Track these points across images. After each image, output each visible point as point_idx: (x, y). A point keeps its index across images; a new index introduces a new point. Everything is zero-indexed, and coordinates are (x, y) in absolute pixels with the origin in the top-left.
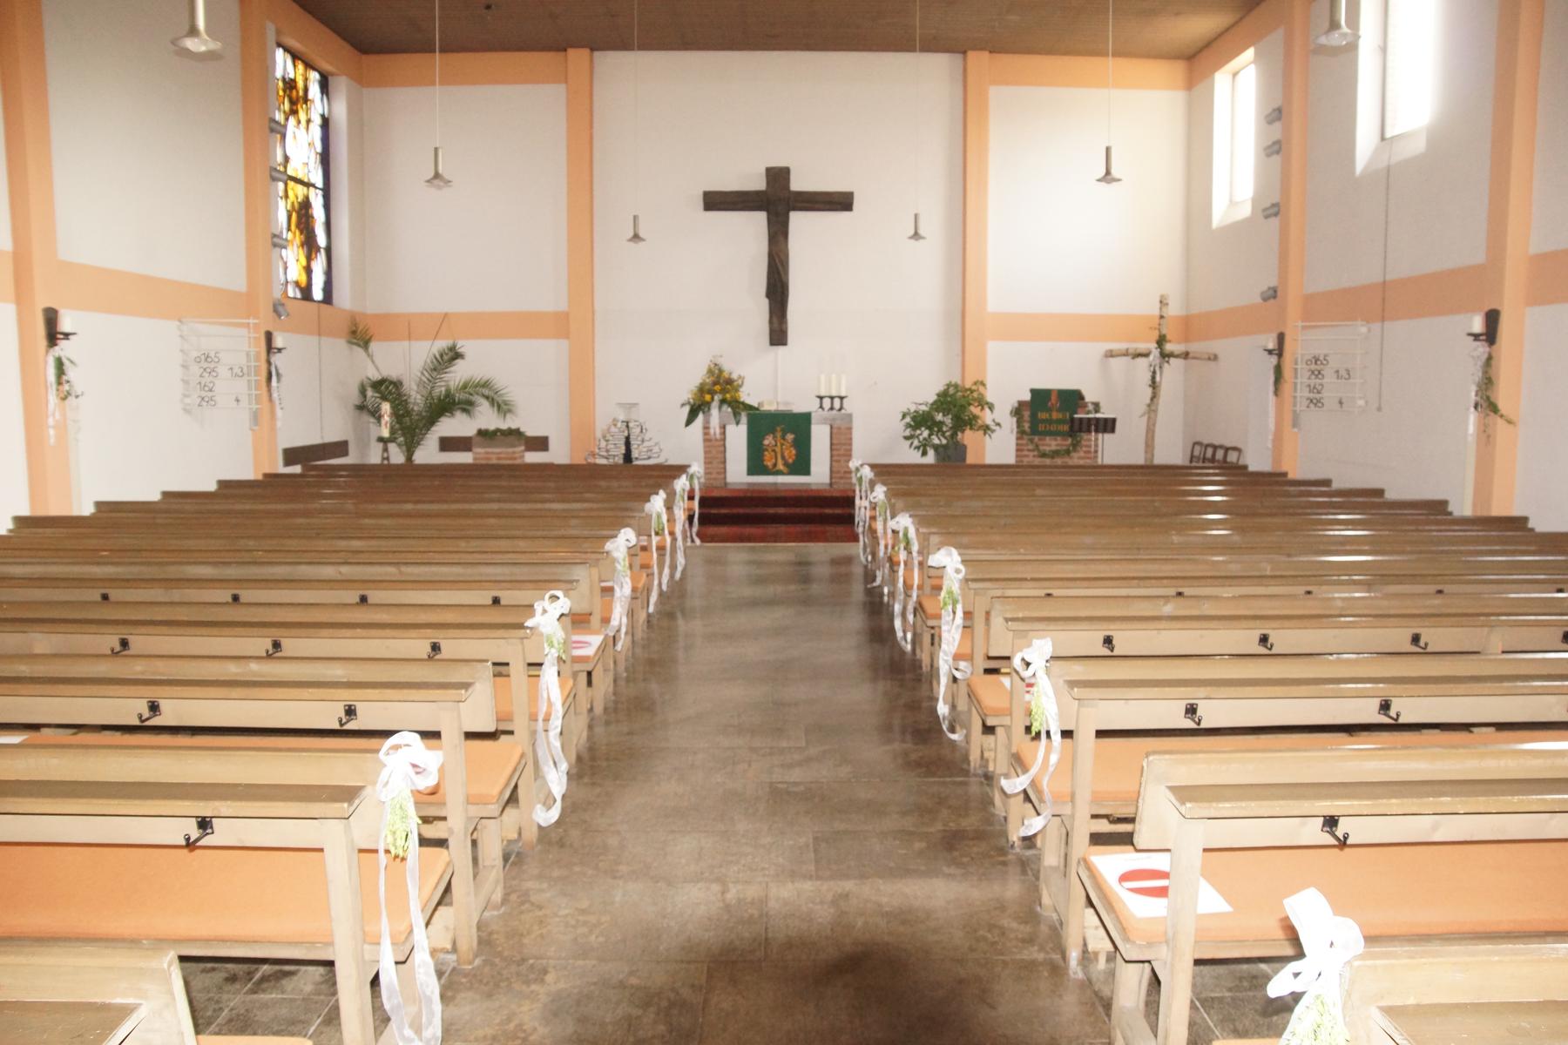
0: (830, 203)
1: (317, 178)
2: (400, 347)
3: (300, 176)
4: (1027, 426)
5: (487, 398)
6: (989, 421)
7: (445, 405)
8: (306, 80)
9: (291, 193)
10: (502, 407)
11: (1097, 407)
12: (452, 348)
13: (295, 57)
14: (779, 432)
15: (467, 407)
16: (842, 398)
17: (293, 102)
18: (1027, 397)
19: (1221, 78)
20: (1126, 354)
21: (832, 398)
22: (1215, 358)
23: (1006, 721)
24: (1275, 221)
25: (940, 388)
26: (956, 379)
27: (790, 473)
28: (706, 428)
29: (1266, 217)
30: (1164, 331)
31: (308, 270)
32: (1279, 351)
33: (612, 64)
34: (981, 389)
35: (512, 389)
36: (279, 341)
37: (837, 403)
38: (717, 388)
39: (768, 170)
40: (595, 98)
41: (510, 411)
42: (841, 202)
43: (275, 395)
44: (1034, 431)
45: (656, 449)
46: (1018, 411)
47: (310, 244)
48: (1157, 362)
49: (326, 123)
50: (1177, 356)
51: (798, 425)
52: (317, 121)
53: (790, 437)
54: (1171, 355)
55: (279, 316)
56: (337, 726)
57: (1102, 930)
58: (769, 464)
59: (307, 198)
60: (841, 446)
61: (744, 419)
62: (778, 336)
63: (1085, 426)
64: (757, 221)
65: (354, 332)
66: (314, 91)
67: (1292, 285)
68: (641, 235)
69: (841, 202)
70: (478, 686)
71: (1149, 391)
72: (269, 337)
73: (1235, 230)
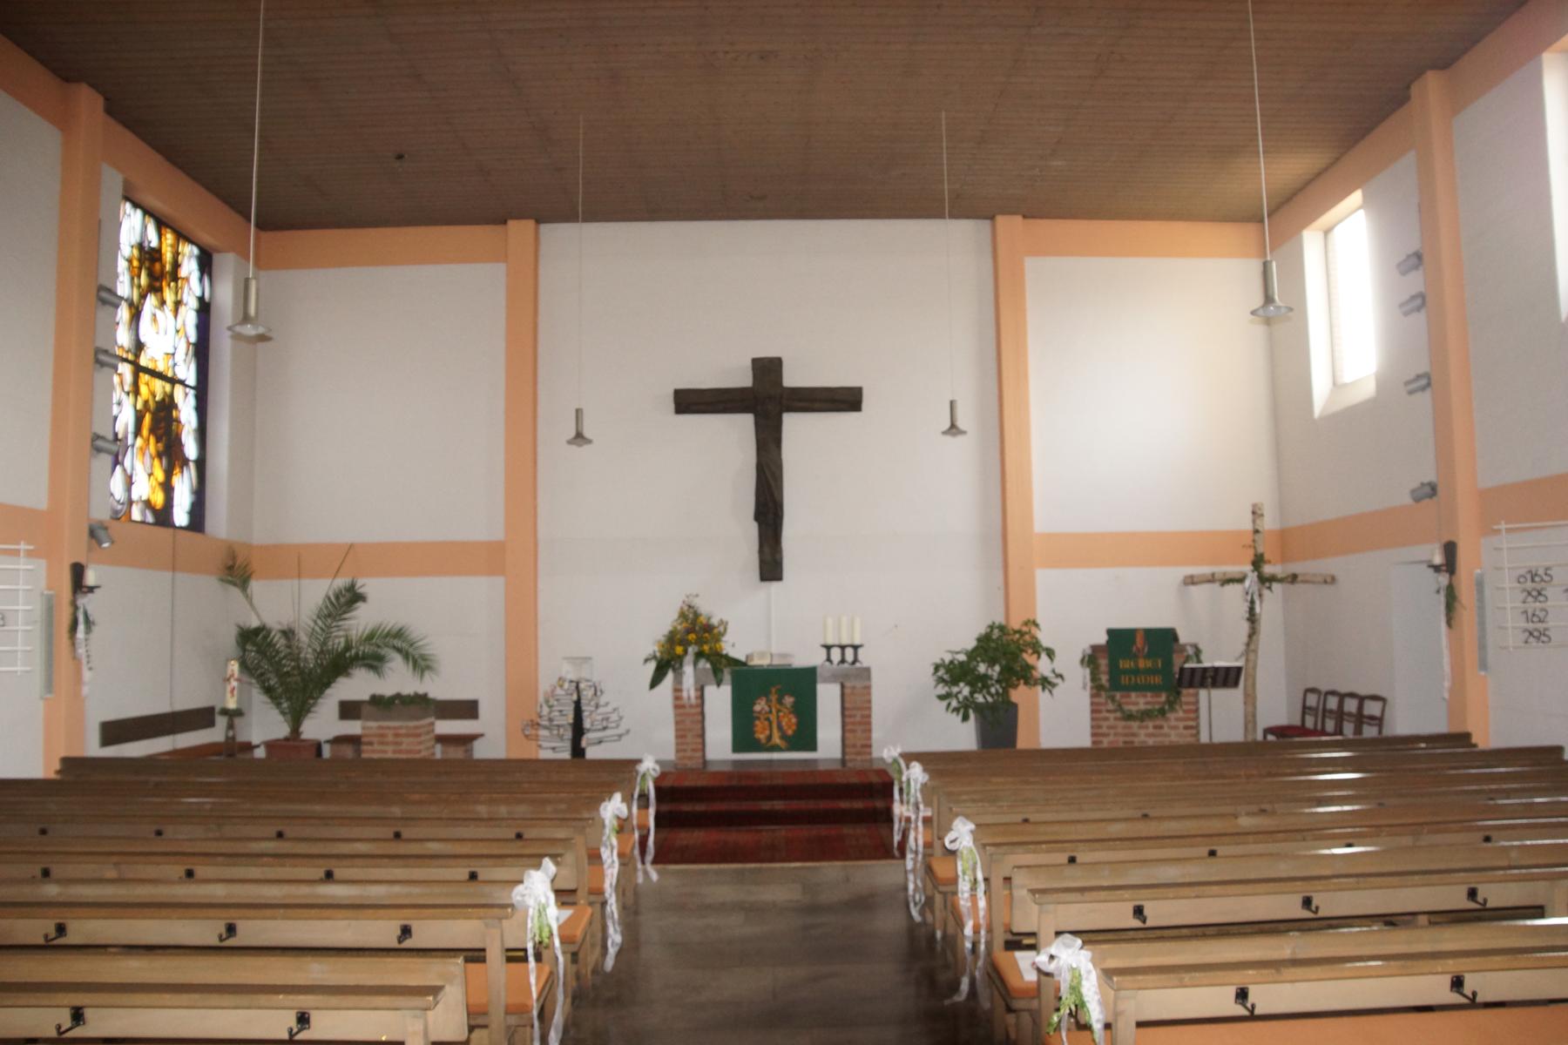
0: (833, 401)
1: (188, 373)
2: (288, 586)
3: (161, 367)
4: (1104, 679)
5: (399, 650)
6: (1048, 674)
7: (339, 664)
8: (176, 254)
9: (144, 390)
10: (420, 663)
11: (1198, 652)
12: (351, 588)
13: (161, 224)
14: (776, 693)
15: (374, 662)
16: (856, 648)
17: (151, 275)
18: (1102, 639)
19: (1311, 239)
20: (1211, 579)
21: (843, 648)
22: (1333, 580)
23: (1035, 1004)
24: (1425, 398)
25: (982, 629)
26: (999, 619)
27: (789, 749)
28: (677, 690)
29: (1411, 393)
30: (1260, 550)
31: (167, 488)
32: (1450, 564)
33: (558, 235)
34: (1034, 630)
35: (435, 643)
36: (90, 578)
37: (849, 653)
38: (692, 637)
39: (755, 361)
40: (541, 271)
41: (429, 668)
42: (847, 400)
43: (81, 651)
44: (1115, 685)
45: (614, 717)
46: (1091, 659)
47: (171, 454)
48: (1255, 588)
49: (204, 309)
50: (1281, 581)
52: (191, 303)
53: (789, 700)
54: (1273, 579)
55: (100, 543)
56: (395, 944)
58: (762, 737)
59: (171, 396)
60: (856, 716)
61: (727, 677)
62: (771, 568)
63: (1197, 678)
64: (741, 427)
65: (230, 568)
66: (189, 267)
67: (1417, 495)
68: (587, 434)
69: (847, 400)
70: (448, 988)
71: (1245, 627)
72: (78, 571)
73: (1350, 419)
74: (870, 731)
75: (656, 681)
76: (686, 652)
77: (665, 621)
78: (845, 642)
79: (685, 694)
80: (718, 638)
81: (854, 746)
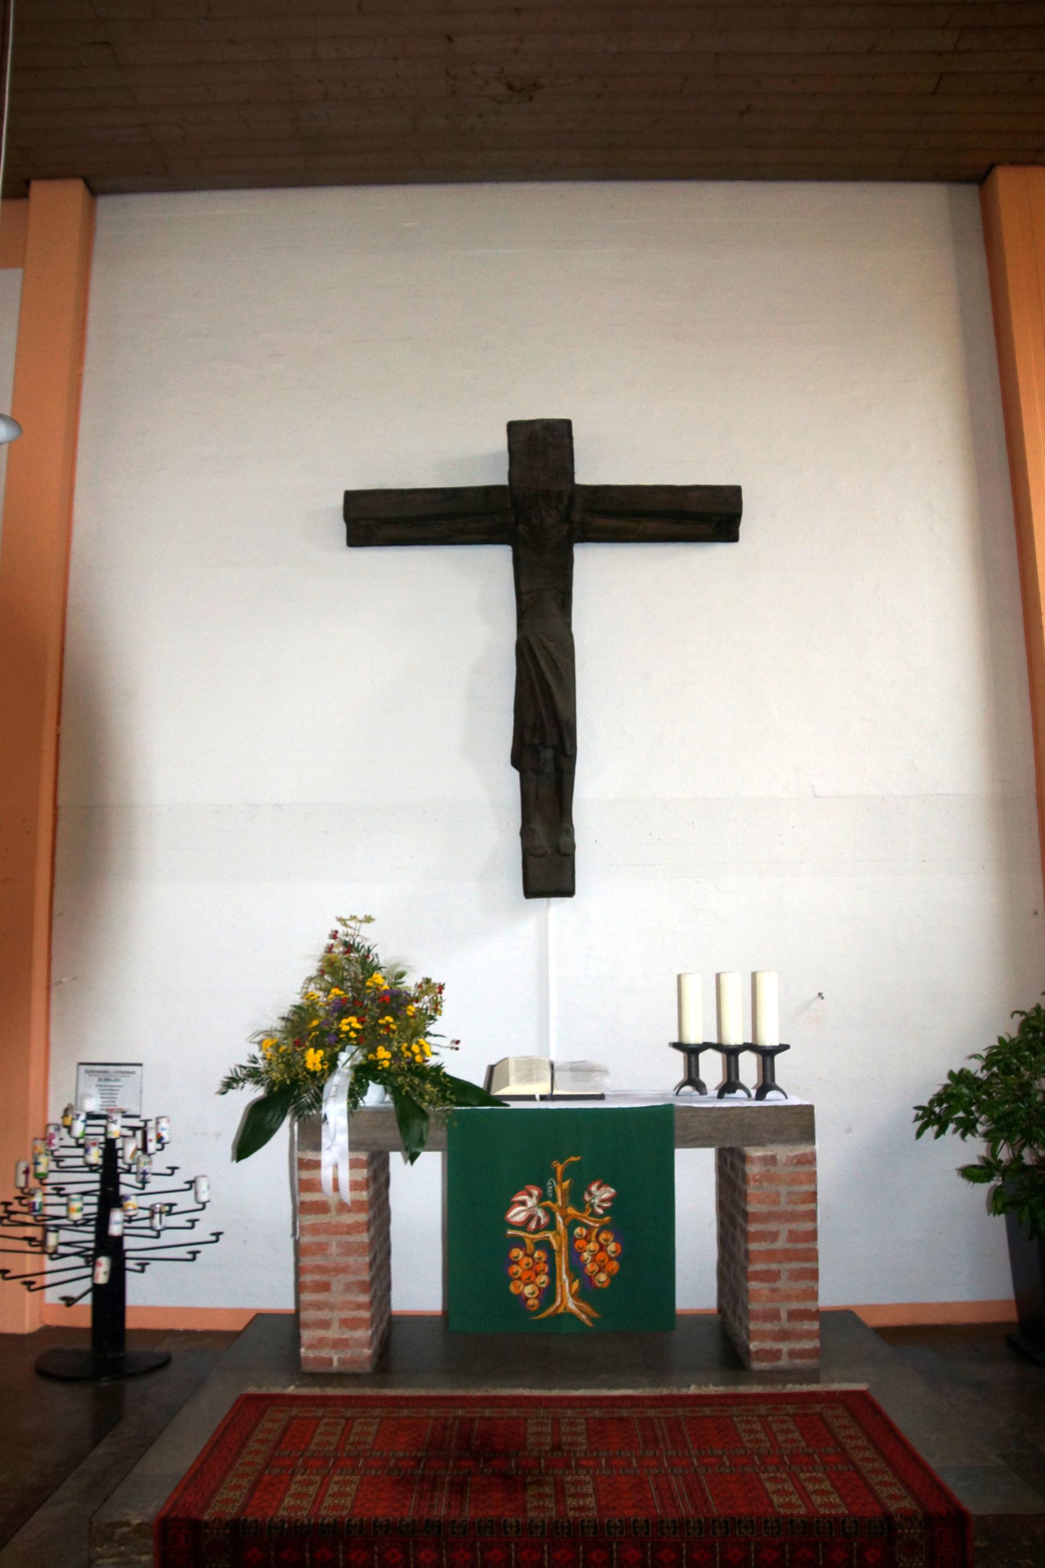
16: (767, 1055)
21: (731, 1053)
28: (304, 1165)
37: (749, 1066)
42: (705, 516)
51: (627, 1147)
53: (601, 1194)
57: (56, 912)
62: (548, 866)
69: (705, 516)
74: (814, 1275)
75: (250, 1139)
76: (332, 1063)
77: (285, 979)
78: (735, 1037)
79: (326, 1174)
80: (416, 1029)
81: (773, 1316)
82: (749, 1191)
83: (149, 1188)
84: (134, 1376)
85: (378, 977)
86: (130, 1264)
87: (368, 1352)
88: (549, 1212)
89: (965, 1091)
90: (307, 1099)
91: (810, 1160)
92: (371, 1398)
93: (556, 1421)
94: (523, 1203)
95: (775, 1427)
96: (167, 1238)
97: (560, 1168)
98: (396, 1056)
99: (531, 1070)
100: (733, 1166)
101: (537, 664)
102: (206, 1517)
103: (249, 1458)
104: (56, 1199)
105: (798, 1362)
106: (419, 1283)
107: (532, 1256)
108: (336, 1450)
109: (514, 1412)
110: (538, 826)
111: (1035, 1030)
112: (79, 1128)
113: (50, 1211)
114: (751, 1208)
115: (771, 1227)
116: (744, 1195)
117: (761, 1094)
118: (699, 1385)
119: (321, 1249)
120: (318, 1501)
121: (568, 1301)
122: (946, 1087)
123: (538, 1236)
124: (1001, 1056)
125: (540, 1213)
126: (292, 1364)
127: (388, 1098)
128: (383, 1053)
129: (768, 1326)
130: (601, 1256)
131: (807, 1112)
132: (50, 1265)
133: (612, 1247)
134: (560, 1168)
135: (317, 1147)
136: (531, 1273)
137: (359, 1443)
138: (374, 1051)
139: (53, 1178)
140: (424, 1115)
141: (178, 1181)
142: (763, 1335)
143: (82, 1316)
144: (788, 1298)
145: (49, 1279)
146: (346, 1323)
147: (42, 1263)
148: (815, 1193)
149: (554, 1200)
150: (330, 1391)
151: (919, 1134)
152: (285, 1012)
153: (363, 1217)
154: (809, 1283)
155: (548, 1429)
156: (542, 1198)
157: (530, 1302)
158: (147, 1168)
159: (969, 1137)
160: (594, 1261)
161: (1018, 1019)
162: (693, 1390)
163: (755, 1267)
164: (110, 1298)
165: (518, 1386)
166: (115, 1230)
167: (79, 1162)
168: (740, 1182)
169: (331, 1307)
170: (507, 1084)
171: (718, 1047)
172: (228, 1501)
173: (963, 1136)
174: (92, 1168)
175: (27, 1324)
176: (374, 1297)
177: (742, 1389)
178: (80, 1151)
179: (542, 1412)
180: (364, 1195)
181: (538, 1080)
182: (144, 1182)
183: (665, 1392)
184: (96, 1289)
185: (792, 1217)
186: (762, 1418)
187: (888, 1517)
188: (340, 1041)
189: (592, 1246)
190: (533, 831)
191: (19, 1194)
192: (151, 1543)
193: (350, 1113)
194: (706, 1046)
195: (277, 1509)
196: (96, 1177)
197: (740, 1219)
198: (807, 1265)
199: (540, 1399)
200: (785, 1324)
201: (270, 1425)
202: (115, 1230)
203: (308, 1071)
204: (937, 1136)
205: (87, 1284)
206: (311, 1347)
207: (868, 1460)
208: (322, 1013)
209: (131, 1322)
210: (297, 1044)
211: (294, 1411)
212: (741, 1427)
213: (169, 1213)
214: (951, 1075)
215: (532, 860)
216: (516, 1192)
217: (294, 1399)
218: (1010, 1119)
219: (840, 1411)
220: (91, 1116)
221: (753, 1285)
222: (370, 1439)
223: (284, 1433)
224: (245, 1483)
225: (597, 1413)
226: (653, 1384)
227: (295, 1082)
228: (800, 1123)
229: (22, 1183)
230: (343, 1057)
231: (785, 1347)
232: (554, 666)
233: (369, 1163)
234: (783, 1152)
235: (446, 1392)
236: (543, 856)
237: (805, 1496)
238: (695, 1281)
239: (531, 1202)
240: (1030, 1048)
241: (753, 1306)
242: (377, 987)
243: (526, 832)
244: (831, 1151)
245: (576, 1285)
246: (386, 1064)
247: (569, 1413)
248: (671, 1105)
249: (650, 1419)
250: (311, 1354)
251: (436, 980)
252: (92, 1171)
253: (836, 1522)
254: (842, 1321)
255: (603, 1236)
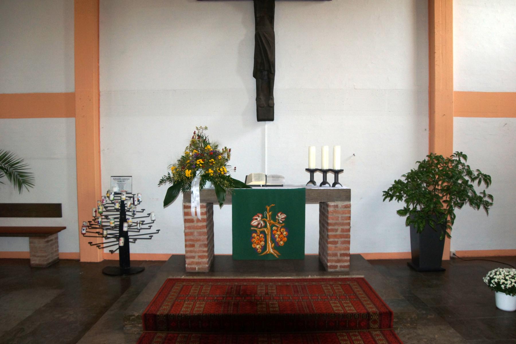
16: (337, 173)
21: (325, 172)
28: (186, 207)
34: (462, 160)
35: (32, 166)
37: (331, 177)
53: (281, 217)
62: (265, 112)
75: (169, 200)
76: (194, 174)
77: (179, 148)
78: (326, 167)
79: (193, 210)
80: (223, 163)
81: (335, 255)
82: (329, 216)
83: (135, 216)
84: (133, 274)
85: (209, 147)
86: (130, 240)
87: (207, 266)
88: (265, 222)
89: (400, 186)
90: (187, 186)
91: (349, 206)
92: (208, 279)
93: (267, 286)
94: (256, 219)
95: (335, 288)
96: (142, 232)
97: (268, 208)
98: (215, 172)
99: (259, 177)
100: (324, 208)
101: (262, 41)
102: (158, 314)
103: (171, 297)
104: (106, 220)
105: (343, 269)
106: (224, 245)
107: (259, 236)
108: (198, 295)
109: (253, 284)
110: (262, 97)
111: (423, 167)
112: (112, 197)
113: (104, 224)
114: (329, 221)
115: (336, 227)
116: (327, 217)
117: (334, 185)
118: (311, 276)
119: (192, 234)
120: (192, 309)
121: (270, 249)
122: (393, 185)
123: (261, 230)
124: (412, 176)
125: (262, 222)
126: (184, 270)
127: (213, 186)
128: (211, 171)
129: (334, 258)
130: (281, 236)
131: (348, 191)
132: (104, 240)
133: (285, 233)
134: (268, 208)
135: (190, 201)
136: (259, 241)
137: (205, 293)
138: (208, 170)
139: (104, 213)
140: (224, 191)
141: (145, 214)
142: (332, 261)
143: (116, 256)
144: (340, 250)
145: (105, 245)
146: (200, 257)
147: (102, 240)
148: (350, 217)
149: (266, 218)
150: (195, 277)
151: (384, 200)
152: (179, 158)
153: (205, 224)
154: (348, 245)
155: (264, 288)
156: (262, 218)
157: (258, 250)
158: (134, 209)
159: (400, 201)
160: (279, 237)
161: (418, 164)
162: (310, 277)
163: (331, 240)
164: (125, 251)
165: (254, 276)
166: (125, 229)
167: (113, 208)
168: (326, 213)
169: (195, 252)
170: (251, 181)
171: (321, 170)
172: (165, 309)
173: (398, 201)
174: (117, 210)
175: (99, 259)
176: (209, 249)
177: (325, 277)
178: (113, 205)
179: (262, 284)
180: (205, 217)
181: (262, 180)
182: (134, 214)
183: (301, 278)
184: (120, 248)
185: (343, 224)
186: (331, 285)
187: (368, 313)
188: (197, 167)
189: (279, 233)
190: (260, 99)
191: (94, 218)
192: (141, 321)
193: (200, 190)
194: (316, 170)
195: (180, 311)
196: (119, 213)
197: (326, 225)
198: (346, 239)
199: (261, 280)
200: (339, 257)
201: (176, 287)
202: (125, 229)
203: (186, 177)
204: (390, 201)
205: (117, 247)
206: (189, 264)
207: (363, 297)
208: (191, 158)
209: (132, 258)
210: (183, 168)
211: (184, 283)
212: (324, 288)
213: (142, 224)
214: (395, 181)
215: (260, 108)
216: (254, 216)
217: (184, 280)
218: (413, 195)
219: (355, 283)
220: (116, 193)
221: (329, 245)
222: (208, 291)
223: (181, 290)
224: (170, 304)
225: (279, 284)
226: (297, 275)
227: (182, 180)
228: (346, 195)
229: (94, 215)
230: (198, 172)
231: (339, 264)
232: (268, 42)
233: (207, 207)
234: (340, 204)
235: (232, 278)
236: (263, 107)
237: (343, 307)
238: (311, 245)
239: (259, 219)
240: (422, 173)
241: (329, 252)
242: (209, 149)
243: (258, 99)
244: (356, 204)
245: (273, 245)
246: (212, 174)
247: (271, 284)
248: (304, 189)
249: (296, 286)
250: (189, 266)
251: (228, 148)
252: (117, 211)
253: (353, 315)
254: (358, 257)
255: (282, 230)
